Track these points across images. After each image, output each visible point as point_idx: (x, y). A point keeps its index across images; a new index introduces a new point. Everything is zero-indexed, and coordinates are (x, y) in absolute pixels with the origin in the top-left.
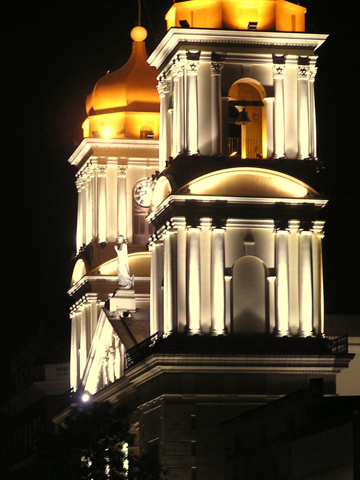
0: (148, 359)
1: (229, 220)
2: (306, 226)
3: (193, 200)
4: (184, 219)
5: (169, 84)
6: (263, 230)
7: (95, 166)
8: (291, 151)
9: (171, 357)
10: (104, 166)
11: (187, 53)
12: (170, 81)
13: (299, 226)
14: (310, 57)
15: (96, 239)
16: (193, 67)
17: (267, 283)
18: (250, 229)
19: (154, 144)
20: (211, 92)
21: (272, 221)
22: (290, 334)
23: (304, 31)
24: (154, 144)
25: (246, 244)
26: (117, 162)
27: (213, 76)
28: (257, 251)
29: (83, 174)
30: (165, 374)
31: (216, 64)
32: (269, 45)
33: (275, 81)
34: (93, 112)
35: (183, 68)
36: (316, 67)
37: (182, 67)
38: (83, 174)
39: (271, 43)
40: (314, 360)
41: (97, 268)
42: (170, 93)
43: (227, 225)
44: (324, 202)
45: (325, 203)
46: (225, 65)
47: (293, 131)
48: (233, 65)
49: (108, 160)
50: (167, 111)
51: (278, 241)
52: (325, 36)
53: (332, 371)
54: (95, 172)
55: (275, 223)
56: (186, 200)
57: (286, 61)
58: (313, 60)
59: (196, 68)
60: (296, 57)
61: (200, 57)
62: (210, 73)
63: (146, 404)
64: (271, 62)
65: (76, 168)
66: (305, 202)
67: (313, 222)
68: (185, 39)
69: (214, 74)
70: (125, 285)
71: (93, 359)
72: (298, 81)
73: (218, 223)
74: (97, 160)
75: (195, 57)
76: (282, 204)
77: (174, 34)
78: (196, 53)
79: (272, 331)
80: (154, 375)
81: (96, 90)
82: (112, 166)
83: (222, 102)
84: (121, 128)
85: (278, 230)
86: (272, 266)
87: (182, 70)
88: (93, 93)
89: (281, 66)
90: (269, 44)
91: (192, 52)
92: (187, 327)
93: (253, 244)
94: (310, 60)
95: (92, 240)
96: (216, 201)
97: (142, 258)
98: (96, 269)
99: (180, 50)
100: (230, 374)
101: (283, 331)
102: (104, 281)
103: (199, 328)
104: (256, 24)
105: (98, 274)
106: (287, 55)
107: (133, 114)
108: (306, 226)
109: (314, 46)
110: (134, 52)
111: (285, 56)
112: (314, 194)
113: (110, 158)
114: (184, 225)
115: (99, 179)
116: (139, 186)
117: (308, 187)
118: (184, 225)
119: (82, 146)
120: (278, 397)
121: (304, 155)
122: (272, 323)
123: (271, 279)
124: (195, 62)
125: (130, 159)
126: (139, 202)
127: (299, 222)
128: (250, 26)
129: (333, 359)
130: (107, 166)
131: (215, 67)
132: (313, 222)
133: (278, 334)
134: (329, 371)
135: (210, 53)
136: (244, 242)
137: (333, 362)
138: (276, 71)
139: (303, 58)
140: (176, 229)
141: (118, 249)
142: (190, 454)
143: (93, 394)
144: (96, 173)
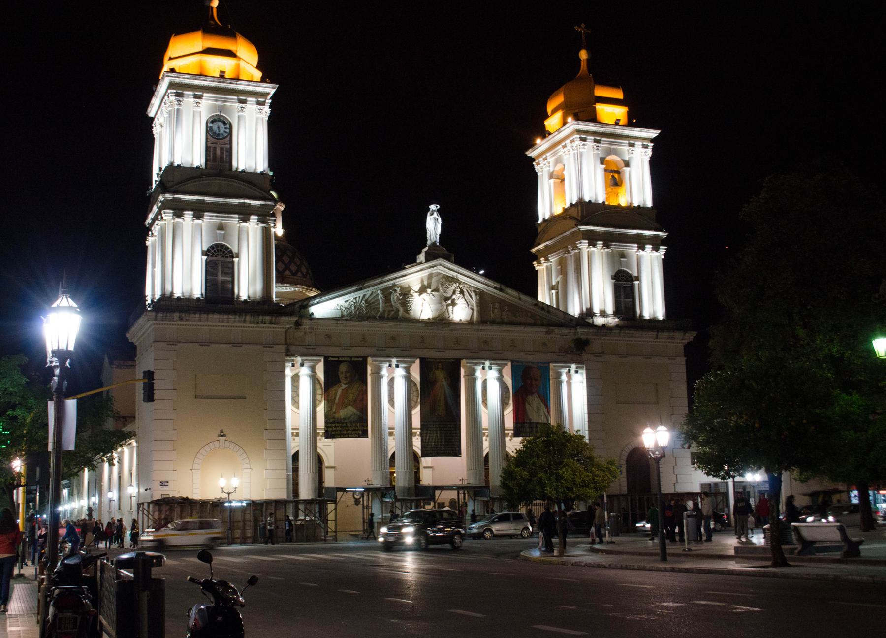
2: (656, 249)
14: (649, 144)
22: (183, 296)
23: (260, 80)
25: (622, 260)
36: (270, 108)
43: (204, 217)
51: (591, 254)
52: (659, 132)
57: (587, 140)
58: (650, 146)
60: (255, 100)
91: (583, 136)
103: (247, 296)
133: (173, 296)
138: (644, 153)
140: (580, 249)
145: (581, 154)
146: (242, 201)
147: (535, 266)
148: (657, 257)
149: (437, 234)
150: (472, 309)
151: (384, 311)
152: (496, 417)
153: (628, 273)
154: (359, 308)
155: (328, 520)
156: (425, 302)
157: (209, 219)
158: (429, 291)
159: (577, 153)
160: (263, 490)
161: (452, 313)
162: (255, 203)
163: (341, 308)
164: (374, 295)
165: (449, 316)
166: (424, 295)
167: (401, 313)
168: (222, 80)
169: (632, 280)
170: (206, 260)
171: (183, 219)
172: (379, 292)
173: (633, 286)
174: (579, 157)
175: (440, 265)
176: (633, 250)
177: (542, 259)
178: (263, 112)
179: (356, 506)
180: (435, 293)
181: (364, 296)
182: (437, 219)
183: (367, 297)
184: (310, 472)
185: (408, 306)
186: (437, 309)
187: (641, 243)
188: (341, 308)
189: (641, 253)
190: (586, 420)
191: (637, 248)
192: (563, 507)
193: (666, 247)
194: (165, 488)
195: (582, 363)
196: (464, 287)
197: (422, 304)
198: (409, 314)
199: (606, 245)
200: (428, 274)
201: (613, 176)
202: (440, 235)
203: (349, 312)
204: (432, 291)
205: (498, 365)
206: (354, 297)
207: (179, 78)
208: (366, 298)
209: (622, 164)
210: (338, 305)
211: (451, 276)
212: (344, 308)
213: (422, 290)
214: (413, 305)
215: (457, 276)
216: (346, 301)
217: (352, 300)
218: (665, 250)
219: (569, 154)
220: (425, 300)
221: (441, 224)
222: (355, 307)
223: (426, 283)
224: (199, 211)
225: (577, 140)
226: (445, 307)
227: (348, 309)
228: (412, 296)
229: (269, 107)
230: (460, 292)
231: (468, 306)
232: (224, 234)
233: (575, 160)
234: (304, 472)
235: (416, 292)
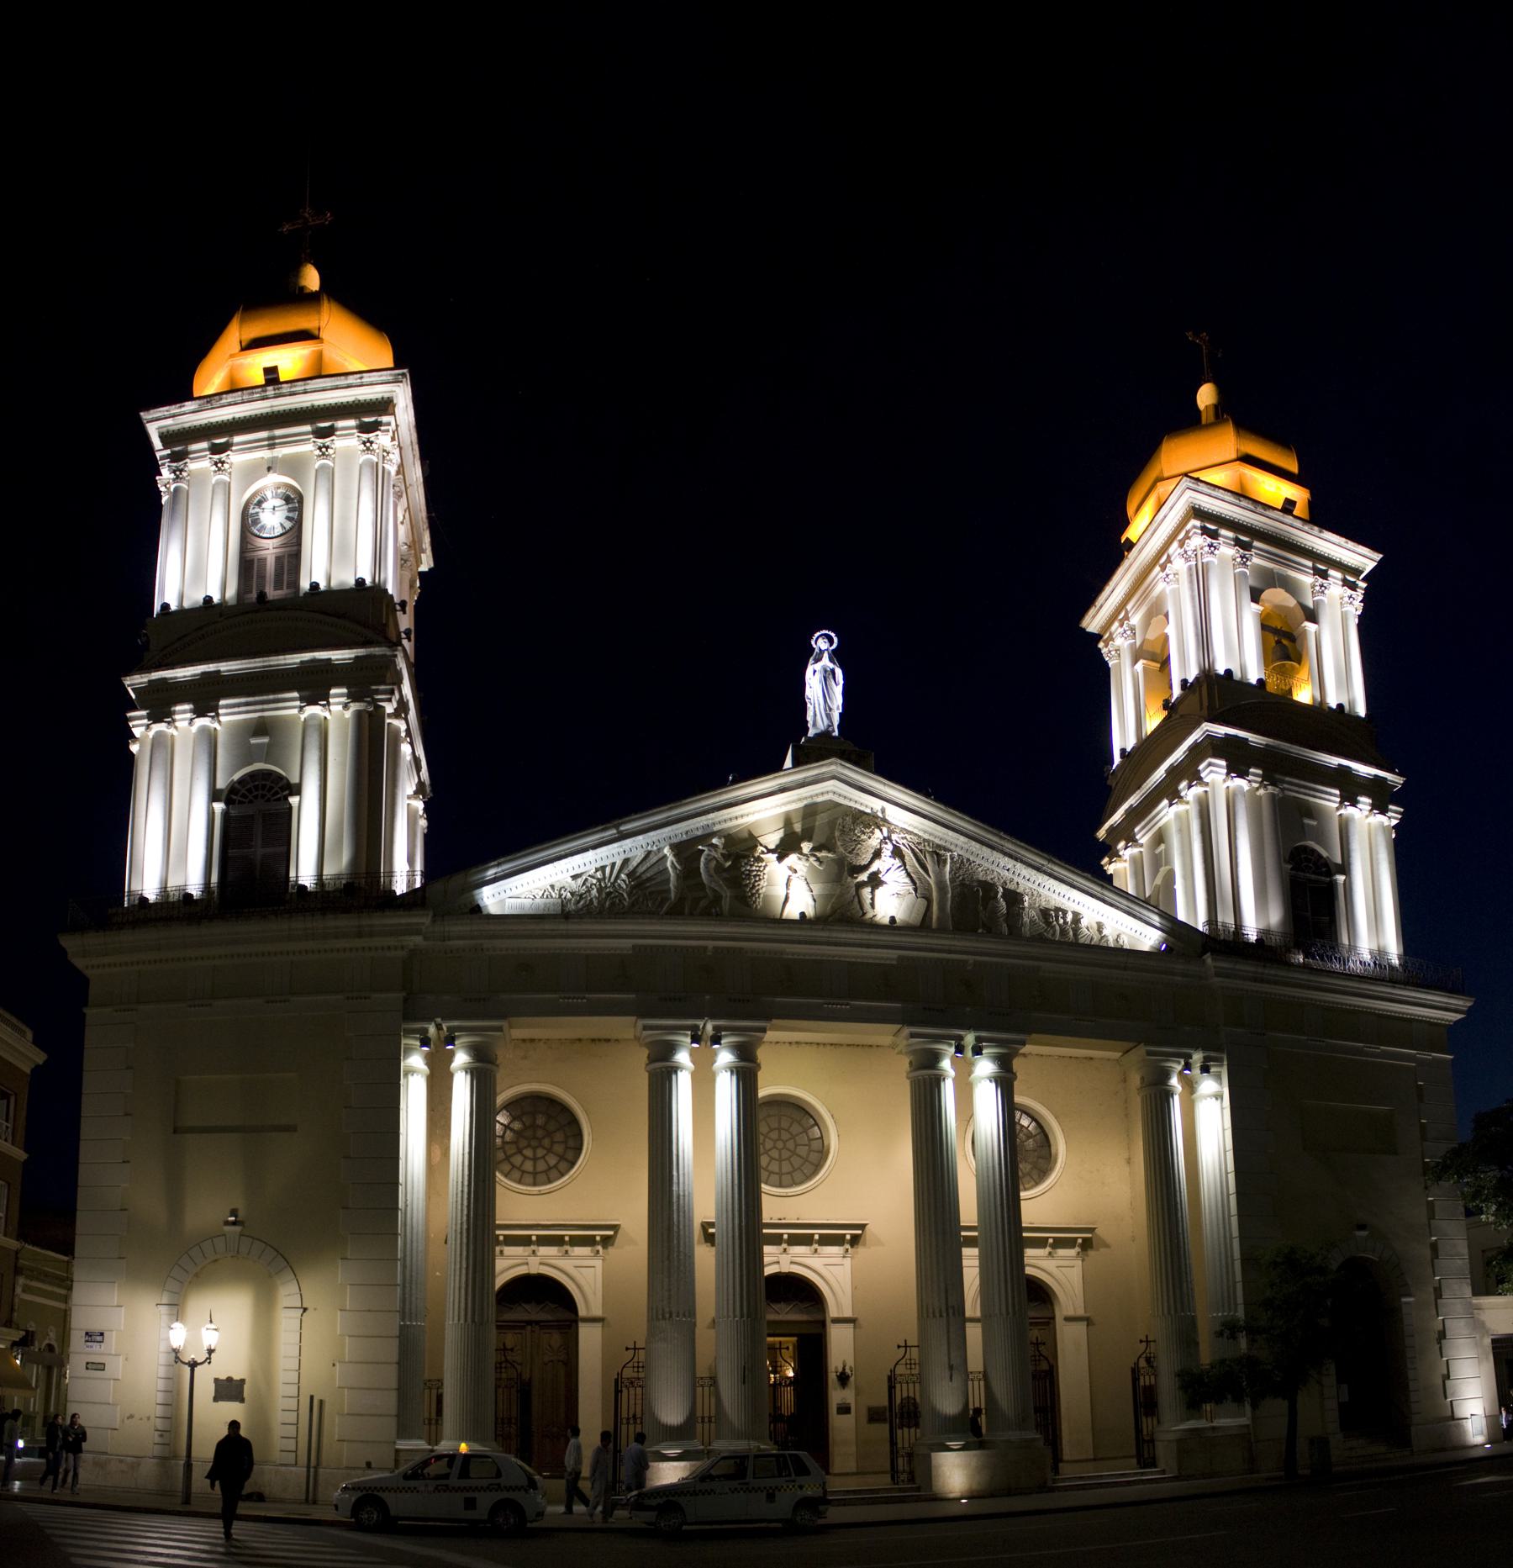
2: (1380, 807)
54: (1196, 555)
58: (1361, 588)
145: (1206, 568)
146: (307, 656)
148: (1384, 829)
149: (830, 709)
150: (929, 900)
151: (681, 899)
152: (993, 1166)
153: (1320, 856)
154: (610, 893)
155: (398, 1389)
156: (794, 876)
157: (230, 715)
158: (806, 847)
159: (1196, 565)
160: (334, 1365)
161: (873, 905)
162: (339, 656)
163: (560, 896)
164: (654, 859)
165: (864, 914)
166: (792, 859)
167: (726, 904)
168: (270, 391)
169: (1330, 874)
170: (226, 815)
172: (666, 851)
173: (1332, 886)
174: (1200, 579)
175: (834, 778)
176: (1329, 801)
179: (233, 1207)
180: (822, 854)
181: (626, 861)
182: (833, 671)
183: (634, 863)
184: (466, 1320)
185: (747, 885)
186: (827, 897)
187: (1350, 789)
188: (560, 896)
189: (1349, 811)
190: (1232, 1188)
194: (96, 1347)
195: (1219, 1049)
196: (905, 841)
197: (789, 880)
198: (749, 906)
199: (1268, 778)
200: (801, 805)
201: (1278, 642)
202: (841, 715)
203: (582, 902)
204: (813, 849)
205: (998, 1043)
206: (598, 865)
207: (173, 416)
208: (631, 867)
209: (1300, 613)
210: (552, 887)
211: (868, 811)
212: (569, 895)
213: (785, 849)
214: (762, 883)
215: (883, 811)
216: (575, 877)
217: (592, 872)
218: (1400, 816)
219: (1178, 580)
220: (795, 871)
221: (844, 685)
222: (600, 890)
223: (798, 827)
224: (204, 698)
225: (1195, 533)
226: (853, 890)
227: (581, 895)
228: (759, 859)
230: (892, 852)
231: (916, 890)
232: (269, 745)
233: (1191, 582)
234: (451, 1322)
235: (769, 851)
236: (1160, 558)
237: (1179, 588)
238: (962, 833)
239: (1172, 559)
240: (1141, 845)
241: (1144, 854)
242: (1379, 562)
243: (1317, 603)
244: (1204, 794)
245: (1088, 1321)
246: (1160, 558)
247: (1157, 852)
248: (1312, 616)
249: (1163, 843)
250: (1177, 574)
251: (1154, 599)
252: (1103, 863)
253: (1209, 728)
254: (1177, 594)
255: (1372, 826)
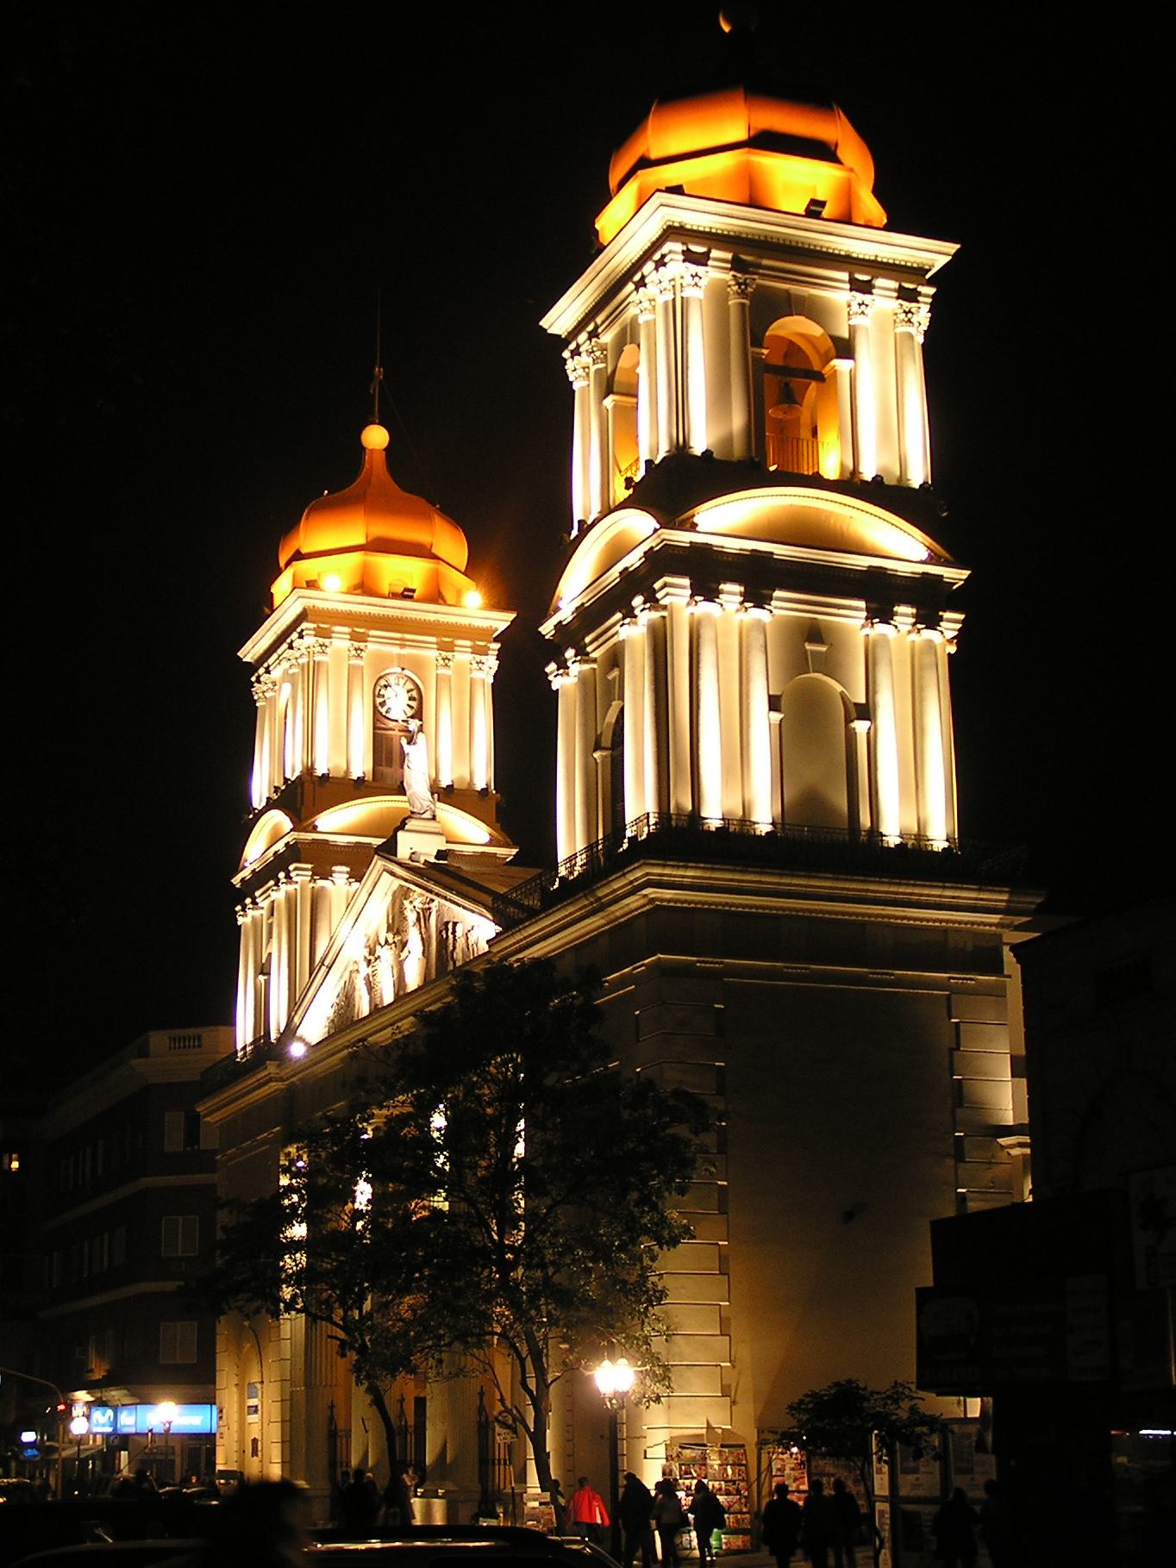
0: (612, 881)
1: (777, 594)
3: (707, 544)
4: (686, 582)
5: (606, 350)
6: (842, 624)
7: (309, 640)
8: (462, 779)
9: (666, 868)
10: (327, 641)
11: (683, 251)
12: (606, 344)
13: (913, 620)
14: (920, 289)
15: (309, 770)
16: (697, 279)
17: (851, 737)
18: (815, 619)
19: (415, 610)
20: (729, 337)
21: (862, 604)
24: (415, 610)
25: (809, 647)
26: (348, 637)
27: (734, 304)
28: (831, 665)
29: (585, 342)
30: (657, 911)
31: (740, 278)
32: (842, 256)
33: (852, 329)
34: (298, 556)
35: (673, 283)
37: (670, 281)
38: (585, 342)
39: (846, 252)
40: (967, 895)
41: (313, 819)
42: (606, 368)
44: (962, 574)
45: (964, 577)
46: (759, 286)
47: (893, 432)
48: (768, 287)
49: (333, 632)
50: (600, 402)
53: (996, 925)
54: (674, 286)
55: (868, 609)
56: (691, 543)
58: (493, 650)
59: (702, 283)
61: (710, 263)
62: (728, 297)
63: (631, 968)
64: (434, 648)
65: (252, 668)
66: (925, 571)
67: (941, 613)
68: (680, 223)
69: (735, 298)
70: (422, 812)
71: (330, 968)
72: (895, 334)
73: (757, 596)
74: (314, 629)
75: (702, 260)
76: (880, 570)
77: (661, 205)
78: (700, 254)
79: (863, 837)
80: (605, 925)
81: (307, 519)
82: (341, 642)
83: (752, 357)
84: (356, 581)
85: (876, 623)
86: (861, 699)
87: (671, 287)
88: (301, 526)
89: (866, 298)
90: (843, 253)
92: (695, 816)
93: (823, 649)
94: (920, 294)
95: (667, 452)
96: (753, 550)
97: (394, 808)
98: (310, 821)
99: (671, 241)
100: (794, 918)
101: (892, 840)
102: (326, 842)
104: (414, 591)
105: (314, 829)
106: (877, 278)
107: (765, 155)
108: (929, 620)
109: (927, 267)
110: (367, 466)
111: (873, 282)
112: (940, 557)
113: (337, 628)
114: (685, 596)
115: (317, 665)
116: (383, 682)
117: (928, 540)
118: (685, 596)
119: (610, 256)
120: (892, 974)
121: (480, 785)
122: (865, 820)
123: (861, 727)
124: (700, 270)
125: (372, 632)
126: (383, 710)
127: (914, 611)
128: (813, 208)
129: (1005, 897)
130: (331, 642)
131: (739, 284)
132: (941, 613)
134: (991, 925)
135: (729, 256)
136: (806, 644)
137: (1004, 904)
139: (908, 289)
140: (665, 608)
141: (409, 743)
142: (713, 1092)
143: (313, 1044)
144: (311, 653)
147: (550, 678)
159: (674, 300)
171: (332, 881)
177: (570, 653)
178: (484, 667)
191: (864, 614)
192: (46, 1438)
193: (962, 617)
229: (495, 657)
236: (631, 275)
237: (655, 320)
238: (353, 603)
239: (647, 281)
240: (594, 661)
241: (597, 671)
242: (954, 256)
243: (852, 330)
244: (661, 620)
245: (271, 1463)
246: (631, 275)
247: (610, 677)
248: (845, 348)
249: (618, 666)
250: (654, 300)
251: (629, 321)
252: (548, 669)
253: (666, 537)
254: (651, 325)
255: (916, 644)
